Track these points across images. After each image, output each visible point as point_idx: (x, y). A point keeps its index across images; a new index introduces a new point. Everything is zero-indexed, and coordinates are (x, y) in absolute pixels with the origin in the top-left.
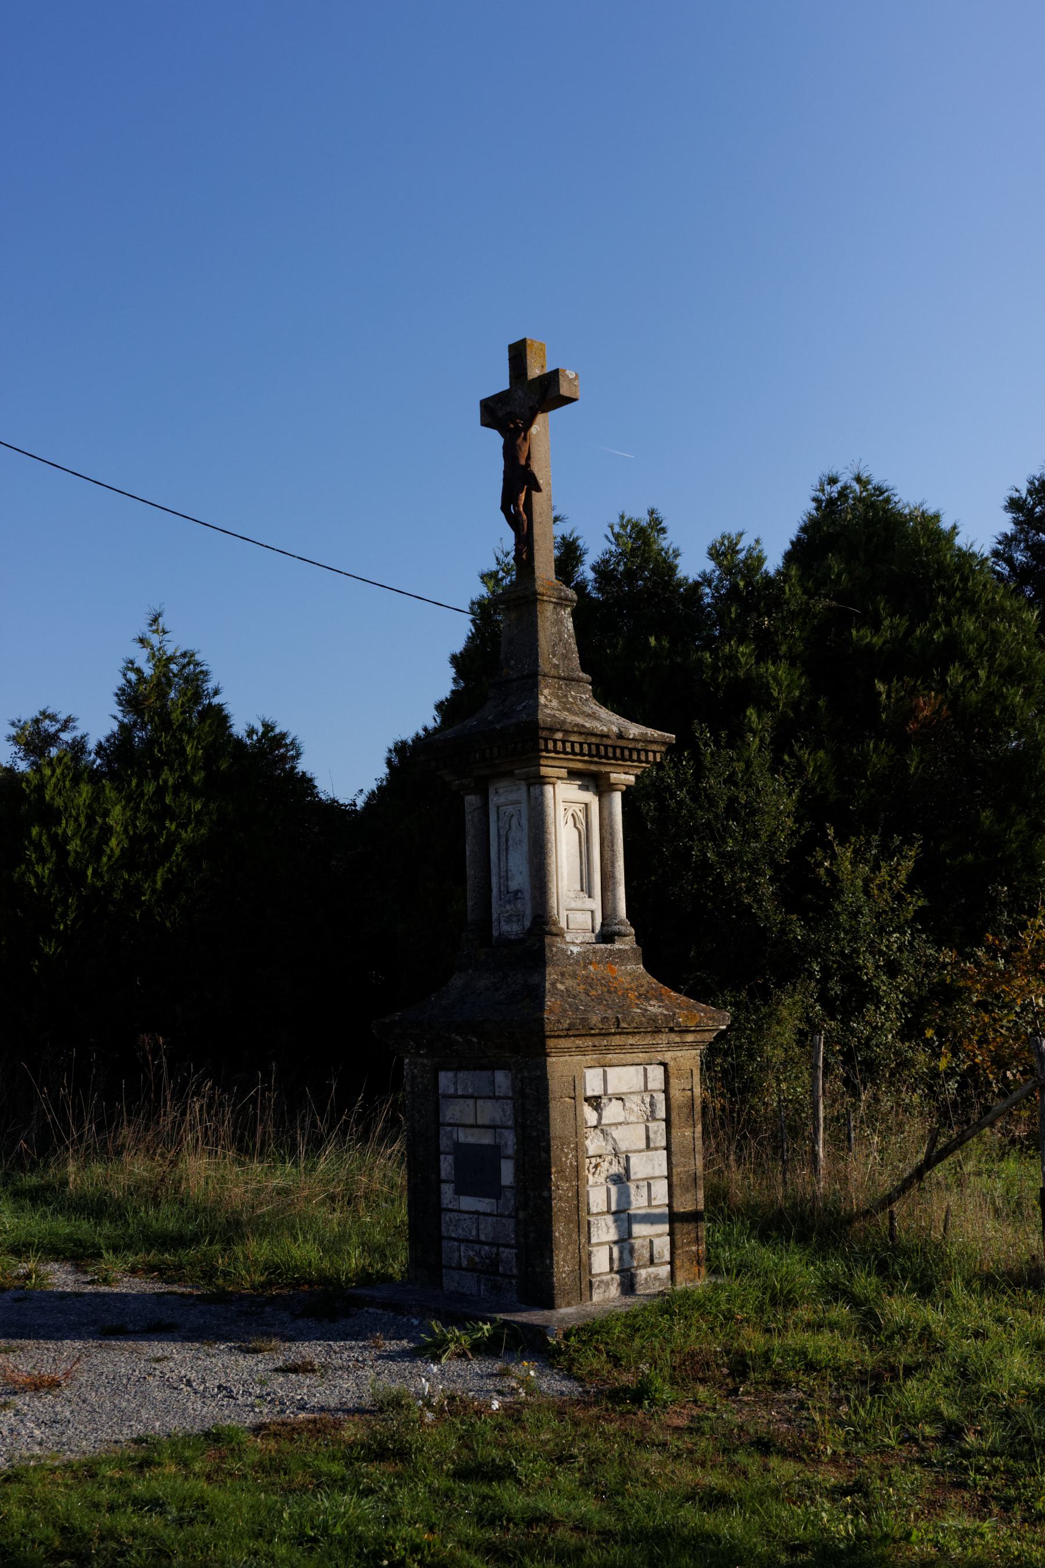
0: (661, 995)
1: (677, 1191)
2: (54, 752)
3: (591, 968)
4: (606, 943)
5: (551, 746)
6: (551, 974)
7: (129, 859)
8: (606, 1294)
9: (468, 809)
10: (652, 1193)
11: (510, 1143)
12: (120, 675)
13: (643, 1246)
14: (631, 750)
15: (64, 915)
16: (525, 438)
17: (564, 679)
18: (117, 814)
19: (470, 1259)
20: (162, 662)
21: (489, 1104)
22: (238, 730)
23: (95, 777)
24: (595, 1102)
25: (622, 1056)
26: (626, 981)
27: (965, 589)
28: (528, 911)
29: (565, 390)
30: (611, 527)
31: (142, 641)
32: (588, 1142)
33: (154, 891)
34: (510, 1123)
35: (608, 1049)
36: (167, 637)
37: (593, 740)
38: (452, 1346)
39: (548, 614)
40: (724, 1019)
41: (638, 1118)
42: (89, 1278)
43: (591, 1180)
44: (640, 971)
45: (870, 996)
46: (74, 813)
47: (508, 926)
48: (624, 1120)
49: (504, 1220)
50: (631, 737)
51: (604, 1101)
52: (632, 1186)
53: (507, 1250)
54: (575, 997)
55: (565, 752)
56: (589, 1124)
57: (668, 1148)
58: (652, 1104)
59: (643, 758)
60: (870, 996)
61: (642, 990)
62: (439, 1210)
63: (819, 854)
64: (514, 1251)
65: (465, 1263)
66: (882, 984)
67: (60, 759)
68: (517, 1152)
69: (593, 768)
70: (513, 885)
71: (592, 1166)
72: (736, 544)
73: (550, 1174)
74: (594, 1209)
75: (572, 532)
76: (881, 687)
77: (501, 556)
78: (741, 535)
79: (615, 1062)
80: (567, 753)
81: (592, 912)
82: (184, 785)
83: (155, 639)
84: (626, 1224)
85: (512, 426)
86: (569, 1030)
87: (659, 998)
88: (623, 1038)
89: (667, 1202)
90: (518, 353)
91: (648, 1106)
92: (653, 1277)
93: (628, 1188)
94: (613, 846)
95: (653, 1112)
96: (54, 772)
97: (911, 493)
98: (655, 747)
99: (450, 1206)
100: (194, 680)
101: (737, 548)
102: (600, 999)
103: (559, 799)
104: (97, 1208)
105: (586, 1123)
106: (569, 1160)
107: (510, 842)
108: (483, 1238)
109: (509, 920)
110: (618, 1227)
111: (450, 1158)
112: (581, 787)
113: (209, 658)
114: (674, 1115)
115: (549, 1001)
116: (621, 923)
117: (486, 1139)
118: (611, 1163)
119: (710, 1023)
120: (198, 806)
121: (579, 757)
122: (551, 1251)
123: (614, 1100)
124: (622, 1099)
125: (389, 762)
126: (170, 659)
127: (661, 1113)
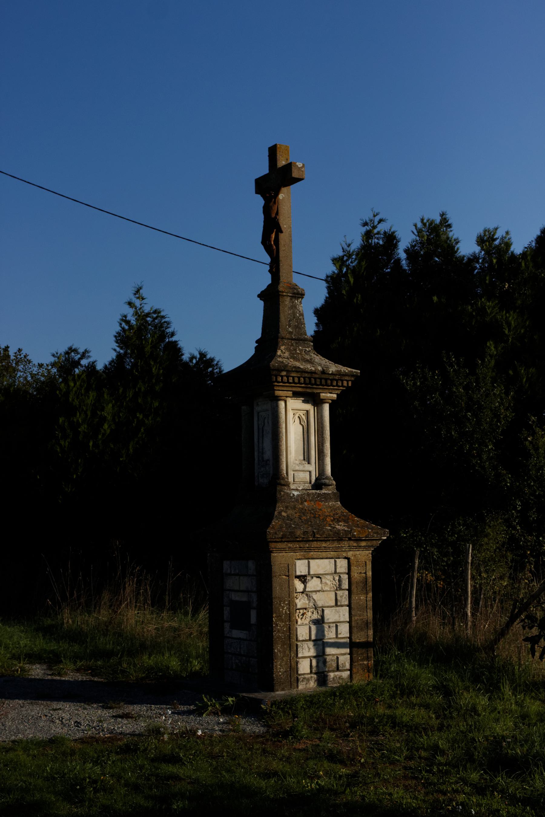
0: (348, 519)
1: (355, 630)
3: (306, 504)
4: (317, 490)
5: (279, 379)
6: (280, 507)
8: (308, 685)
12: (118, 324)
13: (332, 660)
16: (275, 203)
17: (295, 339)
18: (108, 410)
20: (141, 316)
24: (303, 579)
25: (320, 553)
26: (327, 511)
29: (295, 174)
30: (415, 225)
31: (130, 304)
32: (297, 601)
35: (310, 549)
36: (144, 301)
38: (210, 708)
39: (287, 303)
40: (384, 533)
41: (331, 588)
44: (337, 506)
46: (85, 408)
48: (321, 592)
50: (330, 373)
51: (308, 578)
52: (326, 626)
55: (288, 382)
56: (298, 591)
57: (349, 606)
58: (340, 581)
59: (340, 384)
61: (337, 516)
69: (309, 390)
71: (300, 614)
72: (493, 235)
73: (272, 617)
74: (300, 638)
75: (391, 228)
77: (345, 247)
78: (496, 229)
79: (315, 556)
81: (310, 472)
83: (137, 303)
84: (321, 647)
85: (268, 195)
86: (282, 538)
88: (319, 543)
89: (348, 636)
90: (273, 151)
91: (337, 581)
92: (339, 676)
93: (323, 627)
94: (323, 434)
95: (340, 585)
96: (75, 384)
98: (347, 378)
99: (228, 635)
101: (495, 237)
104: (76, 636)
105: (296, 590)
106: (285, 610)
107: (264, 433)
111: (228, 608)
112: (304, 402)
116: (327, 478)
117: (244, 598)
118: (313, 613)
119: (375, 535)
120: (156, 404)
121: (298, 385)
123: (315, 578)
124: (320, 578)
126: (148, 315)
127: (346, 585)
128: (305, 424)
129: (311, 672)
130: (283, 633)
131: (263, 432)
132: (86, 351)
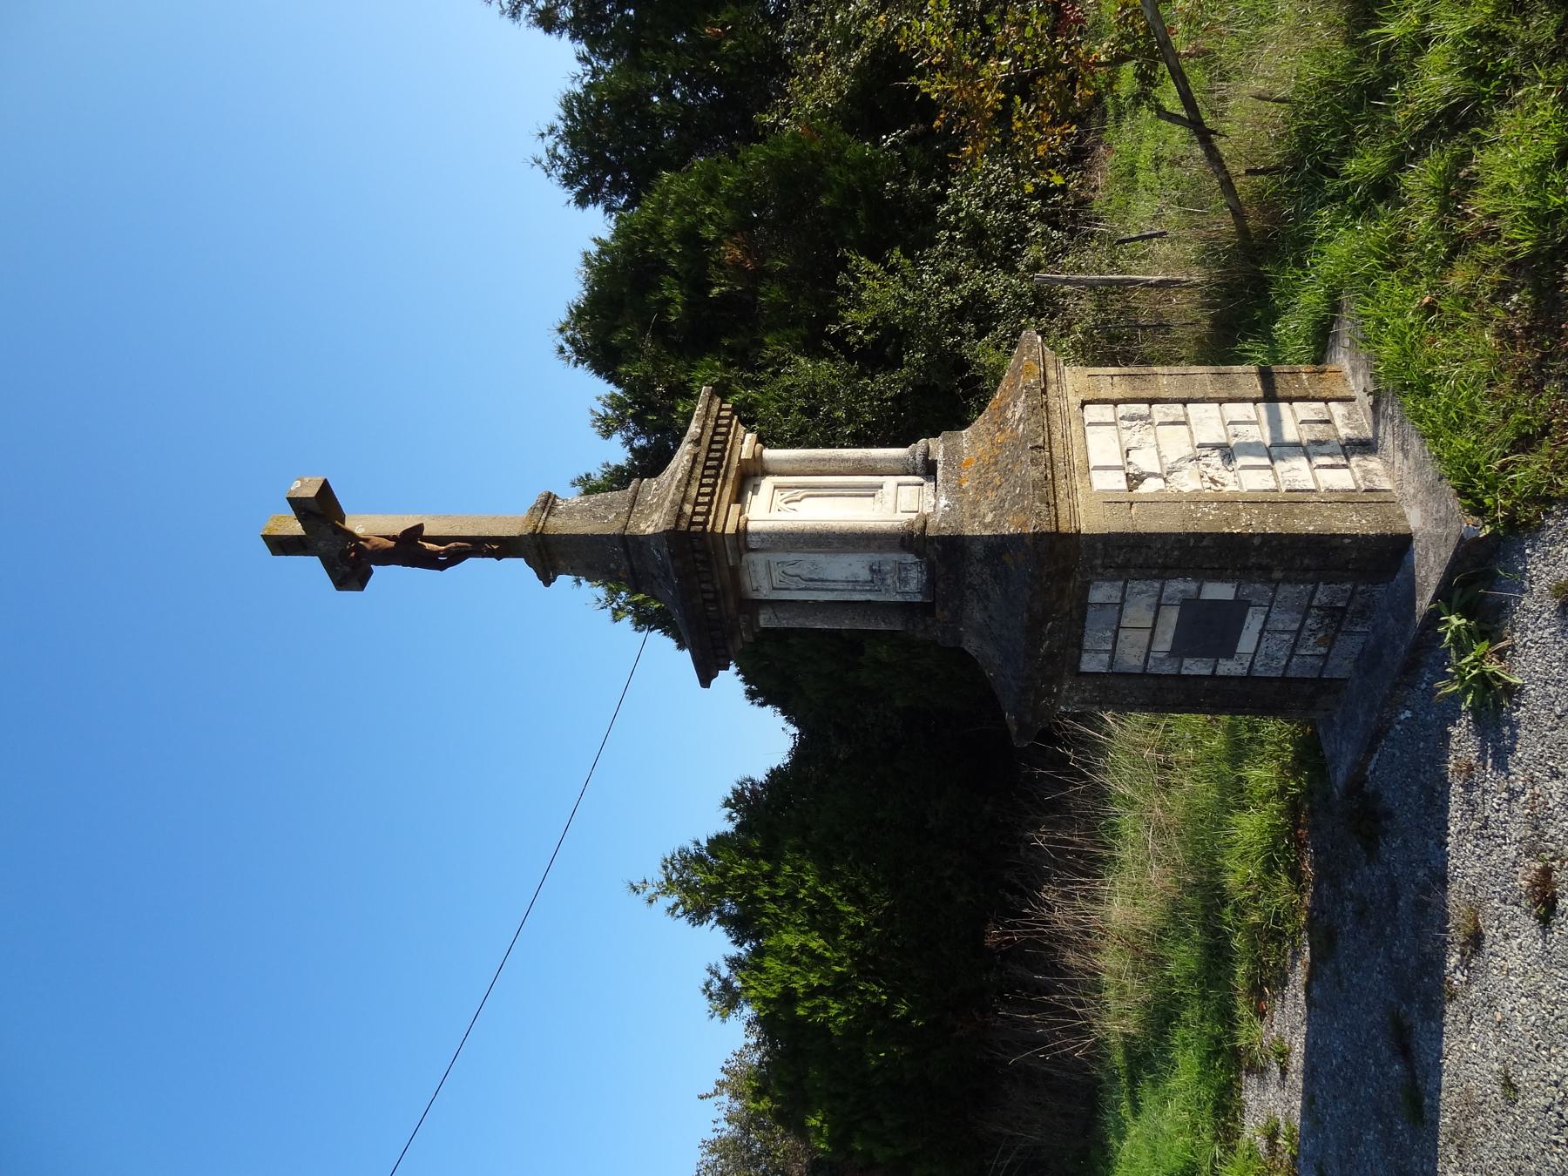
1: (1236, 393)
2: (737, 984)
3: (965, 485)
5: (700, 519)
6: (973, 529)
7: (829, 933)
8: (1374, 471)
9: (774, 624)
10: (1247, 420)
11: (1181, 587)
14: (715, 433)
15: (874, 994)
16: (366, 540)
18: (791, 939)
19: (1318, 643)
20: (668, 887)
21: (1129, 611)
22: (730, 827)
23: (759, 952)
24: (1135, 480)
27: (643, 231)
28: (895, 557)
29: (311, 492)
31: (651, 901)
32: (1186, 490)
33: (856, 914)
34: (1157, 585)
35: (1068, 463)
37: (698, 471)
42: (1276, 1069)
43: (1231, 487)
45: (978, 295)
47: (910, 584)
48: (1151, 451)
49: (1279, 597)
51: (1131, 470)
52: (1233, 442)
53: (1318, 595)
54: (1004, 501)
57: (1185, 402)
58: (1132, 419)
60: (978, 295)
62: (1248, 679)
63: (851, 339)
64: (1321, 586)
65: (1323, 650)
66: (966, 288)
67: (744, 981)
68: (1195, 578)
69: (732, 475)
70: (865, 575)
74: (1272, 485)
76: (716, 291)
80: (711, 502)
82: (769, 877)
83: (651, 890)
84: (1285, 449)
87: (1002, 410)
90: (280, 545)
95: (1141, 418)
97: (572, 288)
98: (715, 408)
100: (689, 861)
102: (1006, 473)
103: (767, 516)
106: (1212, 512)
108: (1295, 626)
109: (904, 581)
110: (1294, 455)
111: (1187, 662)
112: (755, 492)
113: (670, 847)
114: (1144, 395)
115: (1009, 529)
116: (913, 453)
117: (1171, 616)
122: (1334, 536)
125: (762, 705)
126: (668, 879)
127: (1143, 408)
128: (803, 492)
129: (1345, 467)
130: (1265, 515)
131: (812, 580)
132: (710, 970)
